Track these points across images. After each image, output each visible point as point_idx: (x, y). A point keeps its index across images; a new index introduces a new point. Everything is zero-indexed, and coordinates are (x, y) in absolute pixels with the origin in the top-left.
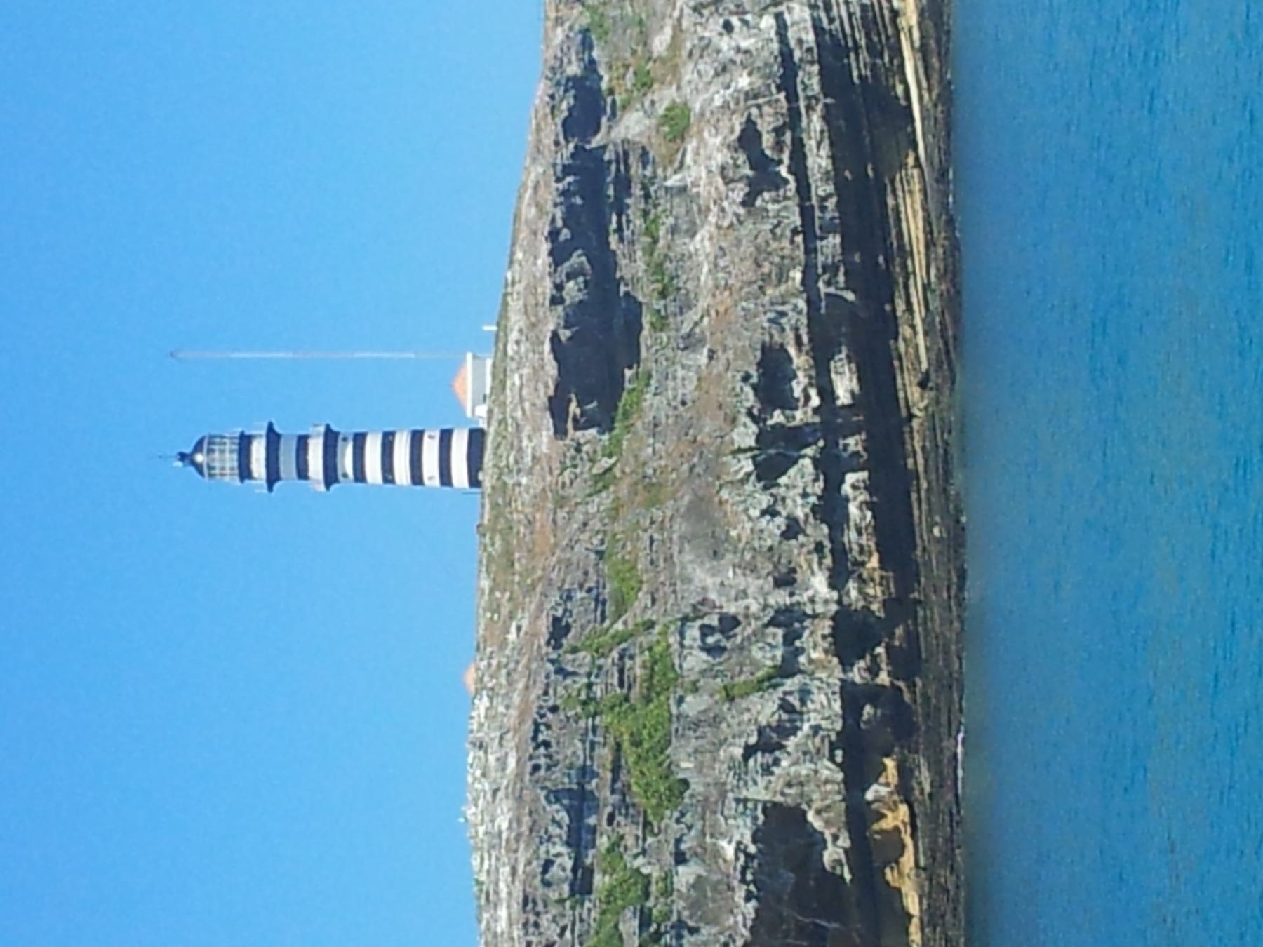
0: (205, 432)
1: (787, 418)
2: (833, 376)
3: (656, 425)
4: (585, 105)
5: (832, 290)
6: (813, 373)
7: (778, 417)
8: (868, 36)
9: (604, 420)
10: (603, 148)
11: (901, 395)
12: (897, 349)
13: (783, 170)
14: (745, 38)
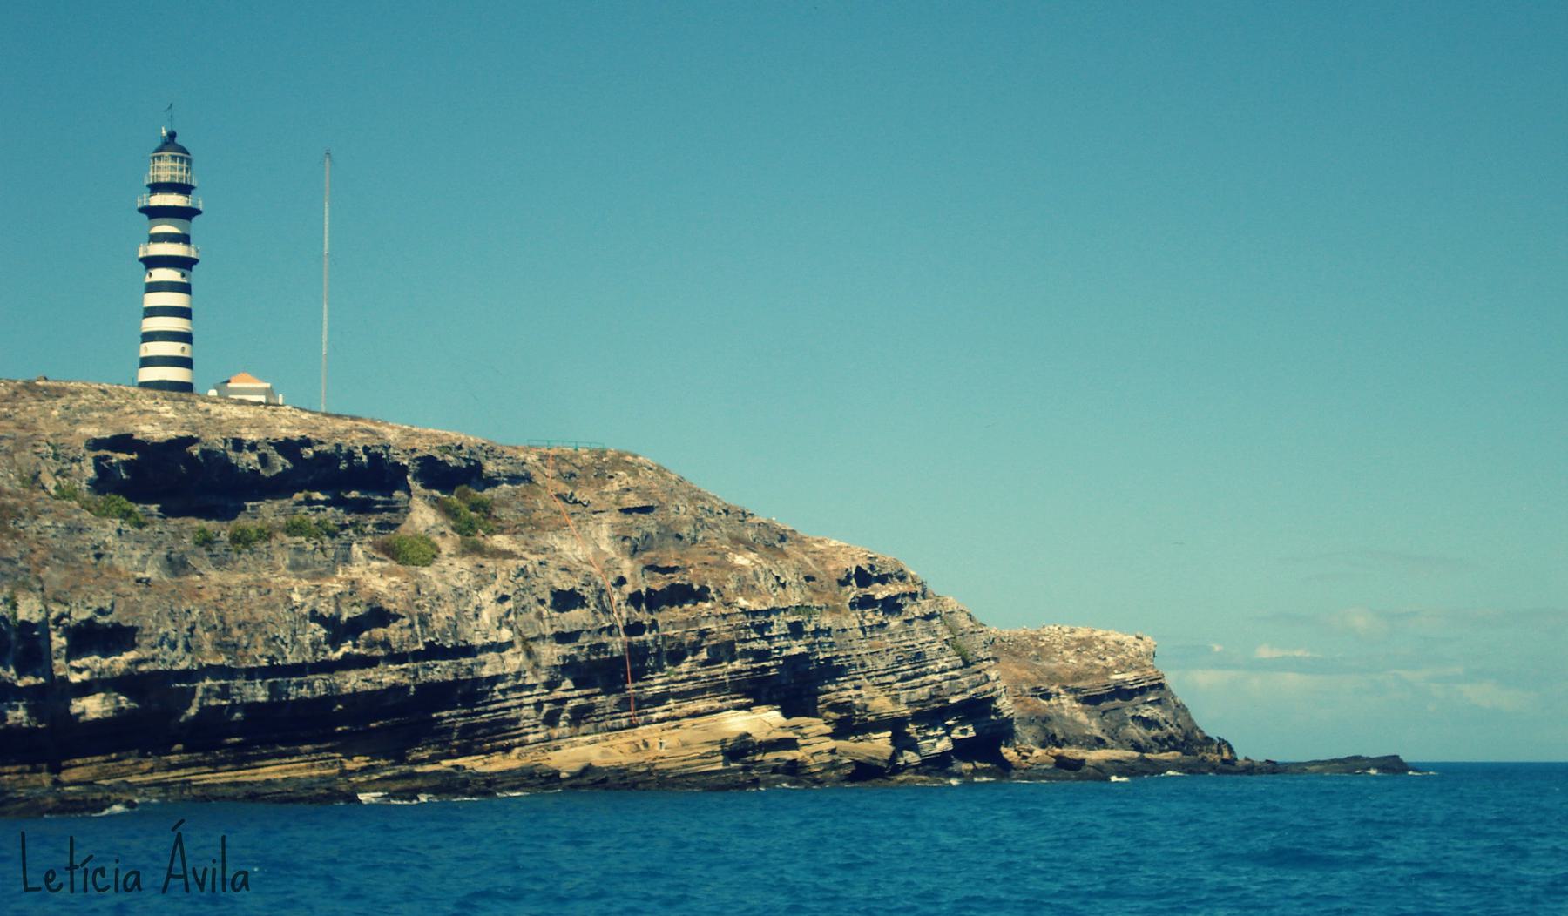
0: (193, 156)
1: (58, 651)
3: (80, 530)
5: (199, 694)
6: (107, 675)
7: (58, 641)
9: (105, 481)
10: (408, 491)
11: (78, 761)
13: (346, 648)
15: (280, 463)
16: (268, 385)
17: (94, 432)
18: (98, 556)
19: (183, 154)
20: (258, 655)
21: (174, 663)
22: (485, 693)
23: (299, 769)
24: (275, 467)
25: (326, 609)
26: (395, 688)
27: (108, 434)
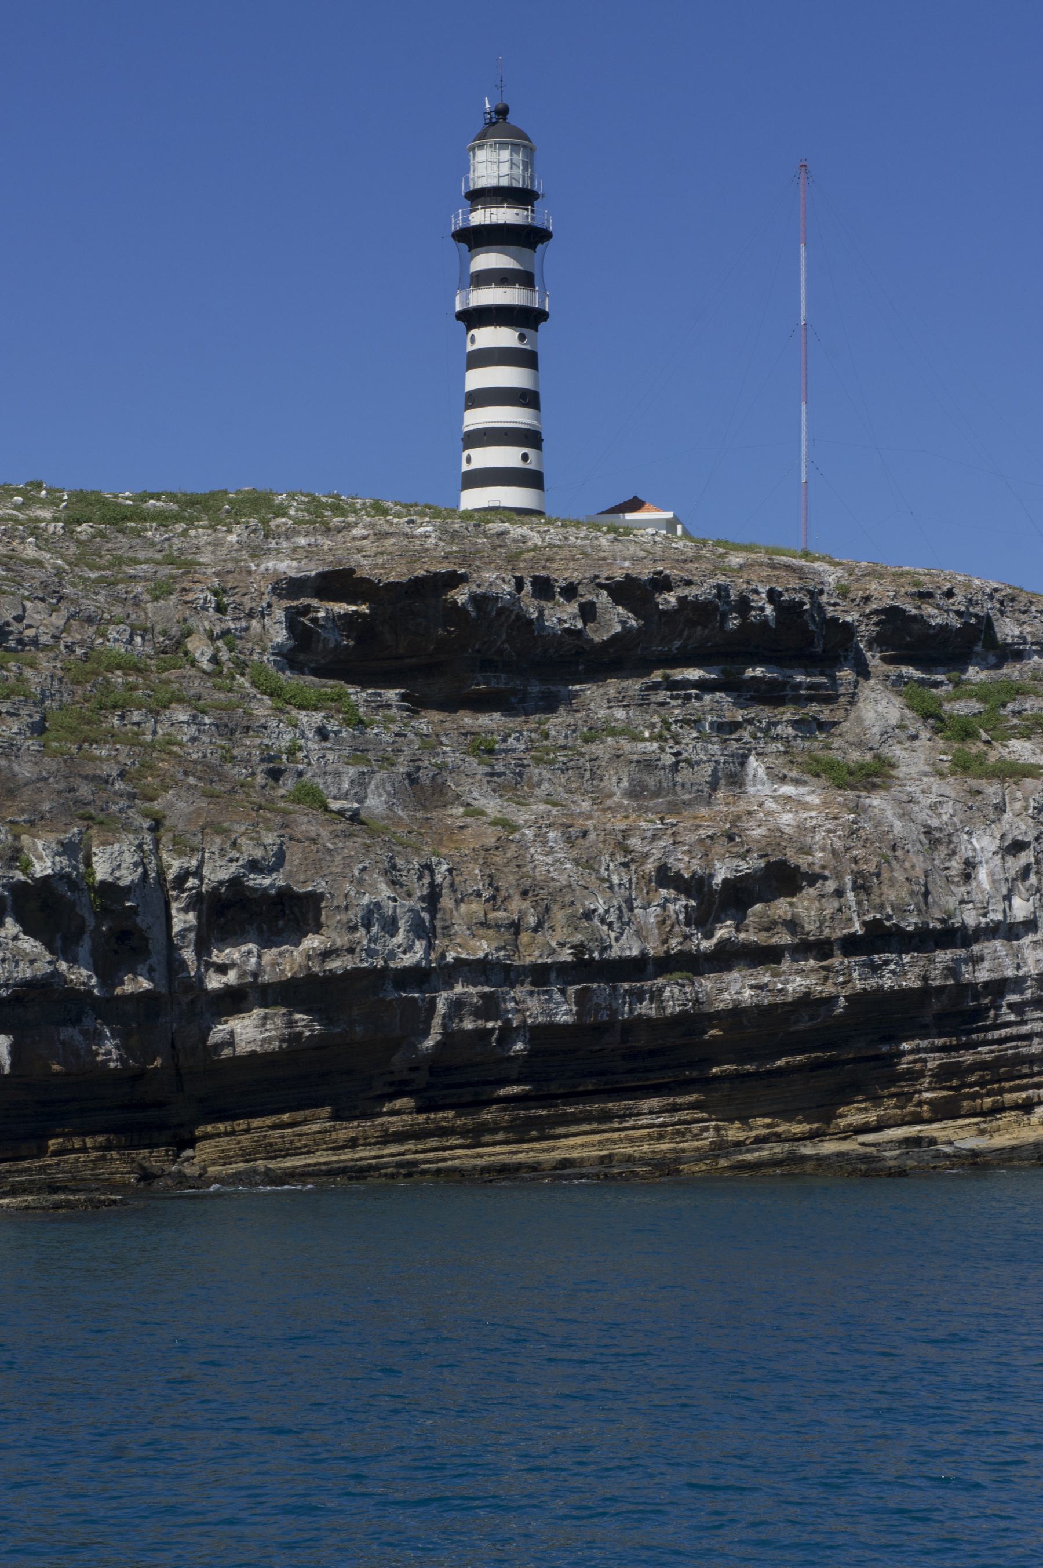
2: (258, 1012)
4: (936, 644)
5: (441, 1008)
7: (182, 920)
8: (983, 1066)
9: (303, 650)
10: (863, 671)
12: (316, 1119)
13: (722, 932)
14: (991, 874)
15: (616, 619)
16: (670, 515)
17: (286, 566)
18: (275, 775)
19: (519, 141)
20: (554, 944)
21: (392, 955)
22: (980, 1013)
23: (632, 1140)
24: (609, 624)
25: (684, 864)
26: (806, 1001)
27: (312, 569)
